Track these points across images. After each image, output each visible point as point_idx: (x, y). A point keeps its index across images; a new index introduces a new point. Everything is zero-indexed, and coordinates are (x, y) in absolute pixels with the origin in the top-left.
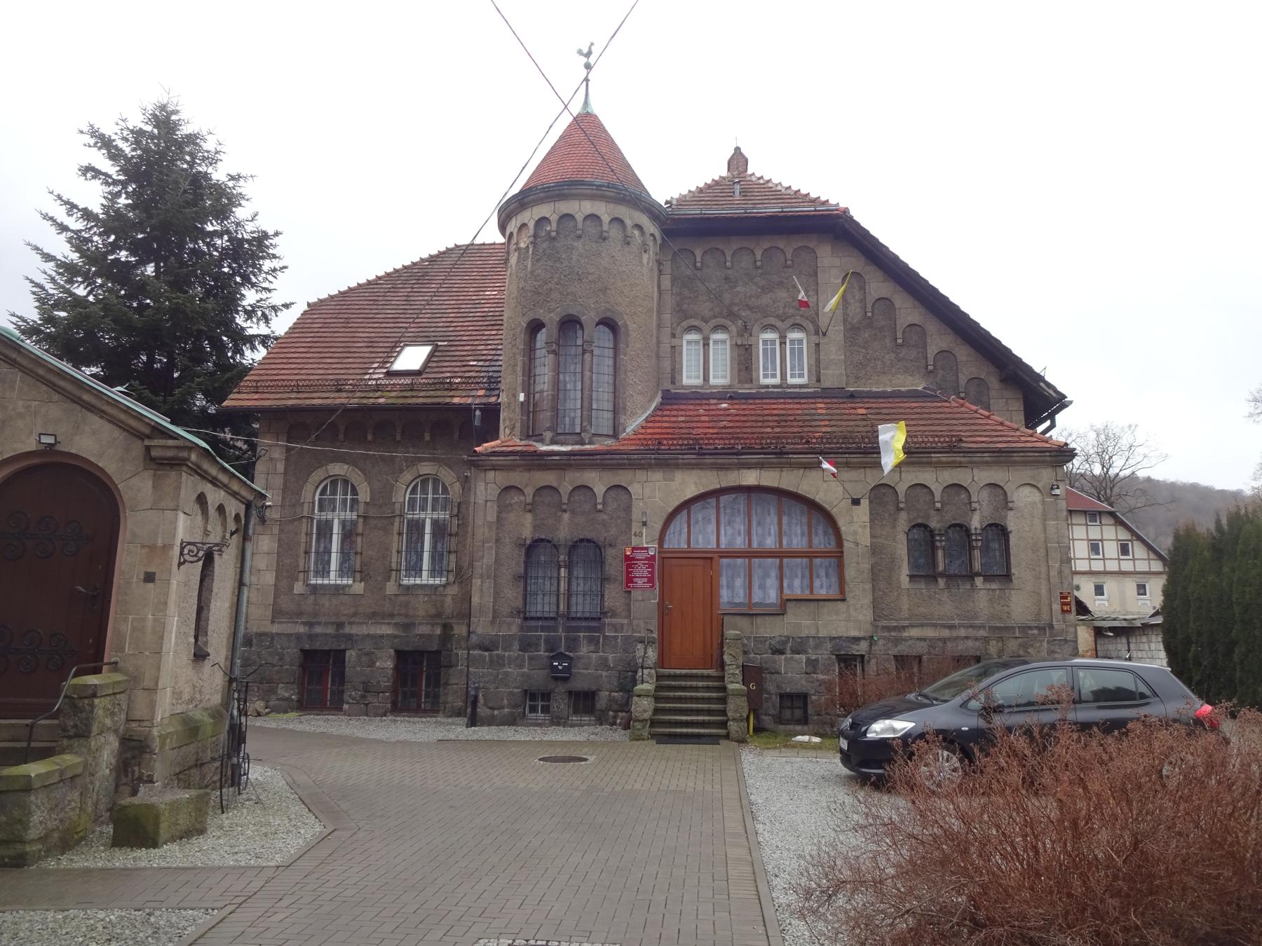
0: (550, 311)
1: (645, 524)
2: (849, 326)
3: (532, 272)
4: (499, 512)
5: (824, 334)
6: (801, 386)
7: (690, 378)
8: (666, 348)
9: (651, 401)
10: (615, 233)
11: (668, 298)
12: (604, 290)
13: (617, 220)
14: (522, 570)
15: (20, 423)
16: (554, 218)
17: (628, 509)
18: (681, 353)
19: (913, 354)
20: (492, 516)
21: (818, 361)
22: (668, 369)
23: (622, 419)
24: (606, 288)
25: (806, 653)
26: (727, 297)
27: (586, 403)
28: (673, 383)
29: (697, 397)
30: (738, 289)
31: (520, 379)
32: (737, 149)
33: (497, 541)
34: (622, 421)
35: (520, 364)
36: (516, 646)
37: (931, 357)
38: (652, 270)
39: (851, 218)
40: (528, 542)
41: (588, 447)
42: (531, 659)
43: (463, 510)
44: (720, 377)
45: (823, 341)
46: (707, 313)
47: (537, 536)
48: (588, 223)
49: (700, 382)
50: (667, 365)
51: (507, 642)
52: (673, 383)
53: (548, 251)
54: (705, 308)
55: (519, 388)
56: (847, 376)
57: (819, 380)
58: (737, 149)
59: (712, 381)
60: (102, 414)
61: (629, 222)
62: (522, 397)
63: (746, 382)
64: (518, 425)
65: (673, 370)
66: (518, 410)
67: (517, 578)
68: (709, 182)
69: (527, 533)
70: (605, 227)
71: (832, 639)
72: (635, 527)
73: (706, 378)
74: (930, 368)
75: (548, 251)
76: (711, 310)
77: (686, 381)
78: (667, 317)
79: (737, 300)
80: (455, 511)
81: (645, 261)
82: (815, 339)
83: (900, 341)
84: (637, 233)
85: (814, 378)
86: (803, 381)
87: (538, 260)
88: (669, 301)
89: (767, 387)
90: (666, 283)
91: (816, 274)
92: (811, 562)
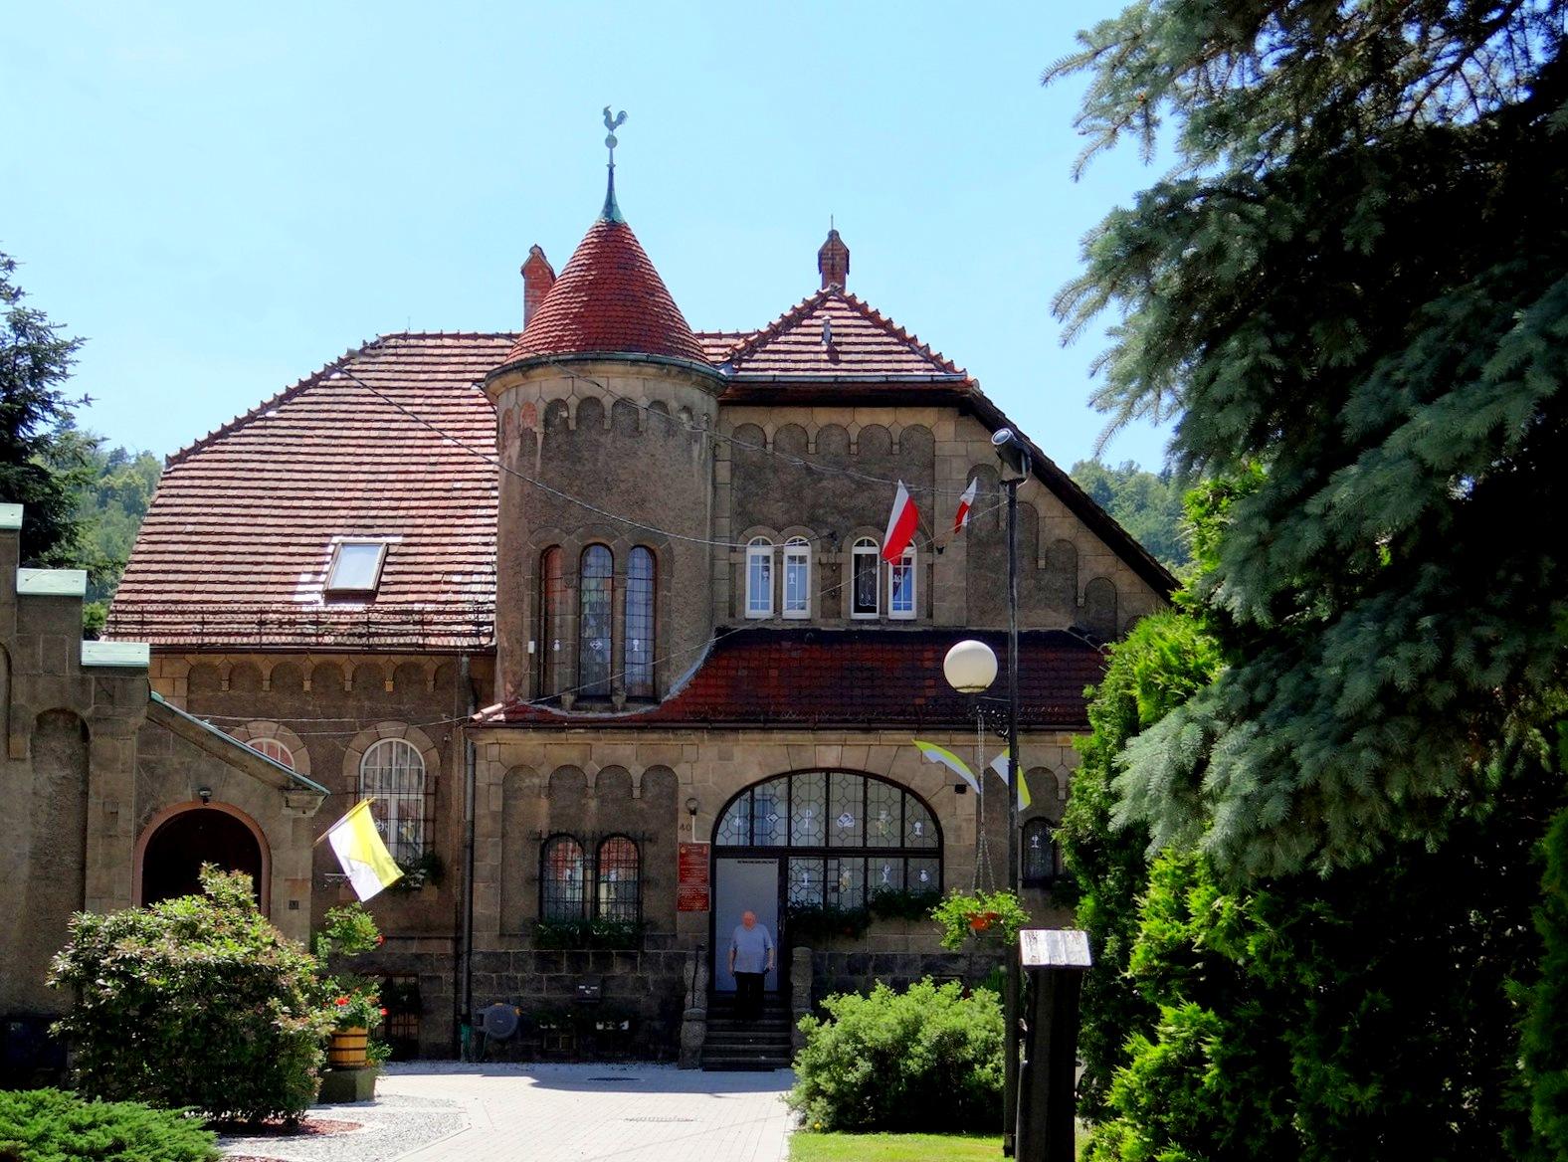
0: (569, 533)
1: (693, 812)
2: (974, 541)
3: (542, 474)
4: (505, 799)
5: (940, 551)
6: (907, 622)
7: (756, 610)
8: (722, 566)
9: (704, 640)
10: (654, 423)
11: (725, 494)
12: (641, 503)
13: (659, 404)
14: (537, 872)
15: (178, 778)
16: (573, 402)
17: (673, 795)
18: (744, 572)
19: (1059, 581)
20: (496, 805)
21: (930, 587)
22: (725, 597)
23: (665, 676)
24: (644, 501)
25: (892, 971)
26: (808, 493)
27: (618, 658)
28: (732, 615)
29: (763, 637)
30: (825, 483)
31: (527, 621)
32: (834, 235)
33: (503, 836)
34: (665, 678)
35: (527, 600)
36: (531, 964)
37: (1082, 585)
38: (706, 460)
39: (981, 394)
40: (544, 836)
41: (620, 715)
42: (550, 979)
43: (442, 788)
44: (799, 608)
45: (940, 560)
46: (781, 519)
47: (555, 830)
48: (620, 410)
49: (768, 613)
50: (724, 590)
51: (519, 961)
52: (732, 615)
53: (565, 447)
54: (776, 510)
55: (527, 634)
56: (969, 610)
57: (930, 615)
58: (834, 235)
59: (787, 614)
60: (244, 768)
61: (673, 405)
62: (531, 647)
63: (832, 616)
64: (526, 683)
65: (732, 597)
66: (526, 662)
67: (530, 881)
68: (788, 313)
69: (543, 825)
70: (643, 415)
71: (923, 957)
72: (683, 817)
73: (778, 608)
74: (1081, 601)
75: (565, 447)
76: (787, 512)
77: (750, 613)
78: (725, 522)
79: (822, 501)
80: (432, 789)
81: (695, 454)
82: (927, 558)
83: (1042, 563)
84: (684, 416)
85: (924, 612)
86: (910, 615)
87: (550, 459)
88: (727, 499)
89: (862, 622)
90: (724, 472)
91: (932, 466)
92: (906, 864)
